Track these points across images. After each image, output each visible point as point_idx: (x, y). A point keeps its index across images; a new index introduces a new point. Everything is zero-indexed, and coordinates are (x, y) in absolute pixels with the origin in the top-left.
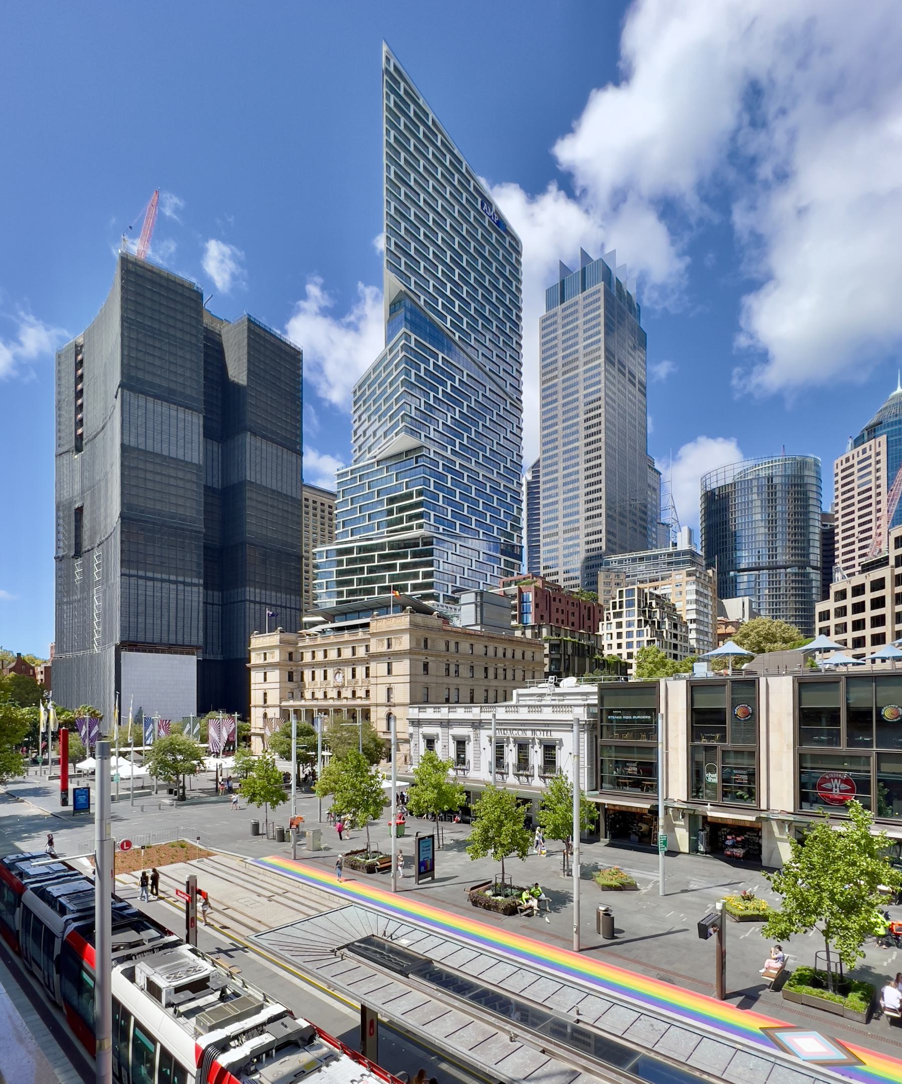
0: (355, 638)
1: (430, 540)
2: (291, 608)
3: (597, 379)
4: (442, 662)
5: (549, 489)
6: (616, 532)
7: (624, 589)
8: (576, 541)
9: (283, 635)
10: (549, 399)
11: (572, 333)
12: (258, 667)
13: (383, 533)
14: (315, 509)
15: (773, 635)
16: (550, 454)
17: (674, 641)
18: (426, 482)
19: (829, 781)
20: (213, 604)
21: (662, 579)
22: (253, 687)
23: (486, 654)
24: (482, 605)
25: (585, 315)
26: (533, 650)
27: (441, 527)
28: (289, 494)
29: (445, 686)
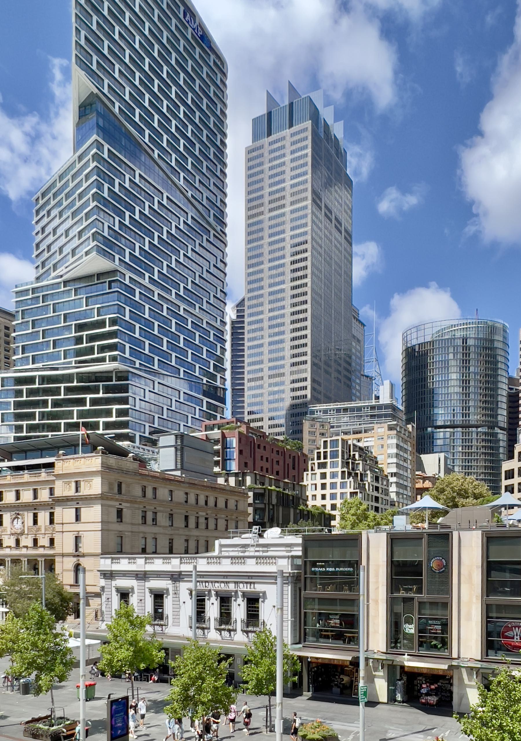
0: (36, 479)
1: (125, 374)
3: (303, 221)
4: (139, 509)
6: (321, 381)
7: (329, 440)
8: (282, 388)
10: (255, 236)
13: (70, 363)
15: (466, 492)
16: (256, 293)
17: (375, 494)
18: (121, 310)
21: (366, 431)
23: (186, 502)
26: (237, 498)
27: (138, 362)
29: (142, 535)
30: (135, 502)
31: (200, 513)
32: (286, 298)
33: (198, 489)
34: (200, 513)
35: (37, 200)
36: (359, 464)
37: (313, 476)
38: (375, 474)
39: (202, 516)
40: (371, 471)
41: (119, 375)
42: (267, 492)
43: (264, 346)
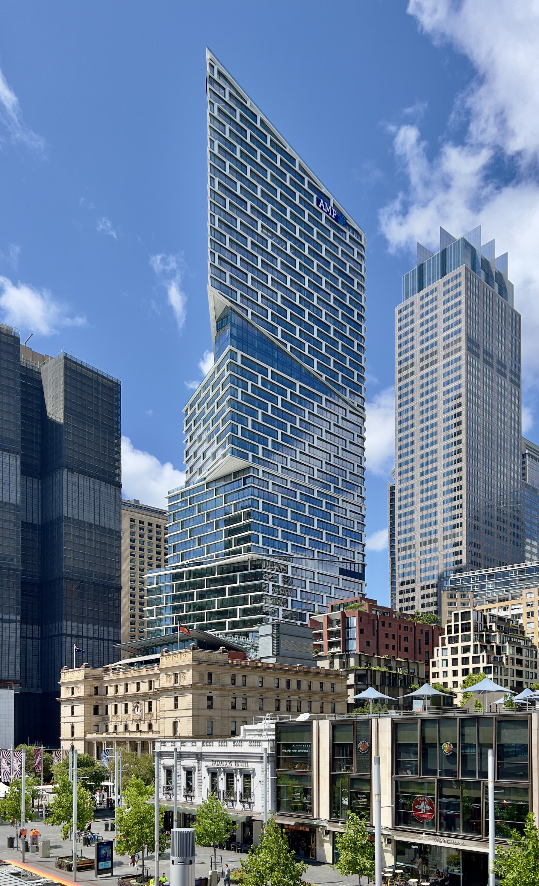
0: (151, 673)
1: (260, 562)
2: (108, 640)
5: (405, 497)
6: (480, 542)
7: (459, 612)
9: (88, 670)
11: (431, 324)
12: (66, 700)
13: (212, 557)
14: (150, 531)
16: (406, 458)
17: (517, 667)
19: (419, 803)
20: (32, 638)
21: (513, 598)
22: (62, 720)
23: (278, 687)
24: (278, 637)
25: (445, 303)
26: (333, 681)
27: (271, 549)
28: (107, 526)
29: (231, 719)
30: (225, 690)
31: (292, 697)
32: (439, 459)
33: (289, 674)
34: (292, 697)
35: (187, 411)
36: (496, 635)
37: (444, 651)
38: (516, 646)
39: (294, 700)
40: (510, 642)
41: (254, 563)
42: (369, 672)
43: (416, 512)
